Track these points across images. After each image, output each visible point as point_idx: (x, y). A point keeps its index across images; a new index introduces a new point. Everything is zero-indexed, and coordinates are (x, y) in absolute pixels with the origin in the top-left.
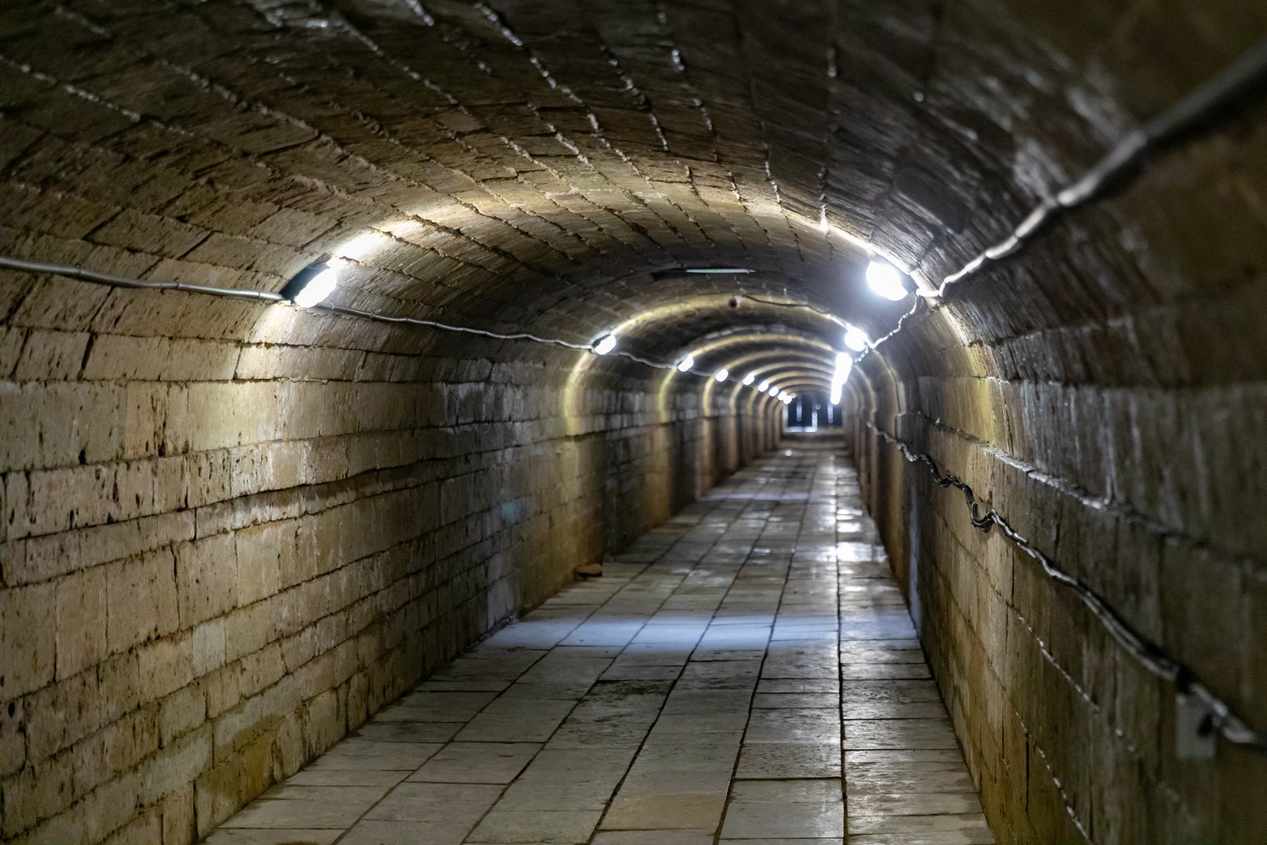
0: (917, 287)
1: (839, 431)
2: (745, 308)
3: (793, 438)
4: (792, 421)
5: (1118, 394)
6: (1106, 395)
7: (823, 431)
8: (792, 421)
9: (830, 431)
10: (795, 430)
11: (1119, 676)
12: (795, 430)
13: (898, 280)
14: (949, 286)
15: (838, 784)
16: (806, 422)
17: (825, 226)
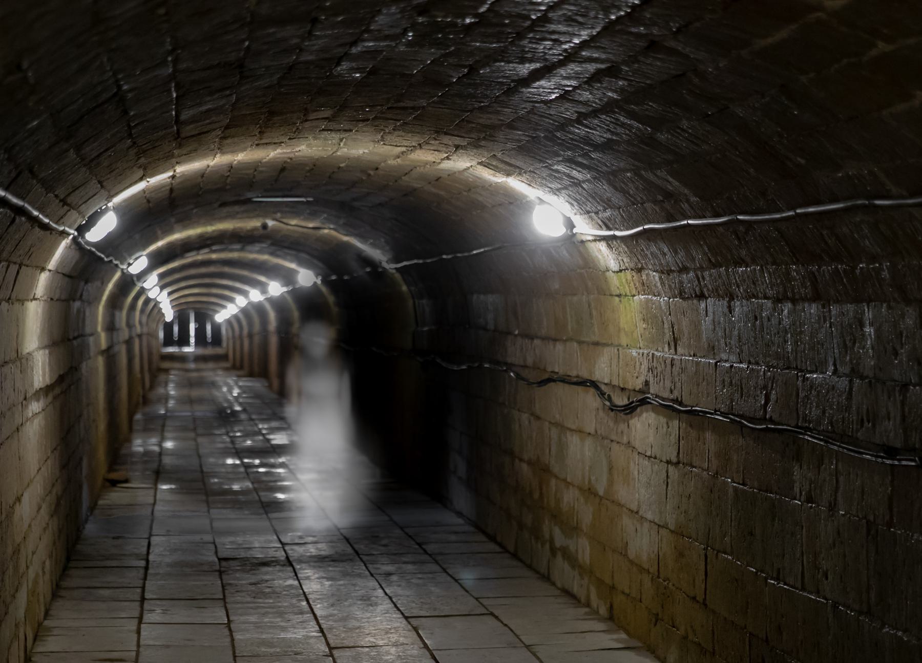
0: (574, 227)
1: (219, 351)
2: (275, 231)
3: (171, 357)
4: (169, 341)
5: (850, 308)
6: (834, 309)
7: (201, 351)
8: (169, 341)
9: (209, 351)
10: (171, 350)
11: (841, 479)
12: (171, 350)
13: (561, 220)
14: (107, 257)
15: (221, 603)
16: (183, 340)
17: (463, 164)
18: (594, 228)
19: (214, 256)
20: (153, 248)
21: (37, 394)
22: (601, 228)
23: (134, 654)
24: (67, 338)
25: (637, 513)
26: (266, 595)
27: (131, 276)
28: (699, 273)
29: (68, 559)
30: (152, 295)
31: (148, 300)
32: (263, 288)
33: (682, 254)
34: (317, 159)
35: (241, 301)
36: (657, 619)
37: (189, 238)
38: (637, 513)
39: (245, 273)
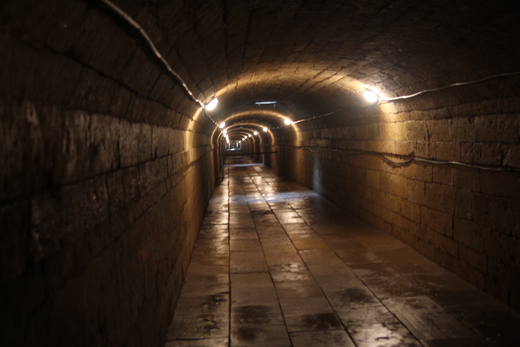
18: (390, 97)
19: (241, 124)
20: (228, 119)
21: (192, 164)
22: (394, 96)
23: (228, 255)
24: (200, 144)
25: (407, 199)
26: (269, 226)
27: (220, 129)
28: (450, 108)
29: (205, 214)
30: (224, 136)
31: (223, 137)
32: (247, 135)
33: (409, 107)
34: (284, 81)
35: (246, 137)
36: (419, 239)
37: (236, 117)
38: (407, 199)
39: (242, 132)
